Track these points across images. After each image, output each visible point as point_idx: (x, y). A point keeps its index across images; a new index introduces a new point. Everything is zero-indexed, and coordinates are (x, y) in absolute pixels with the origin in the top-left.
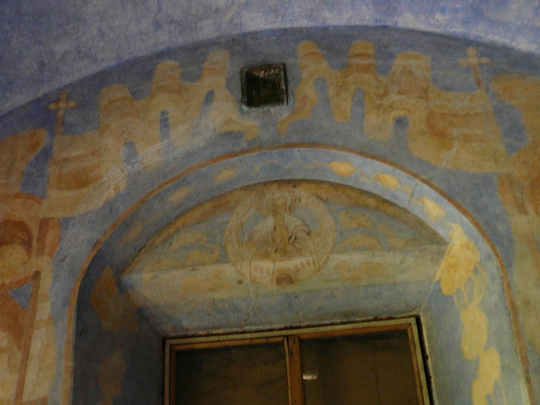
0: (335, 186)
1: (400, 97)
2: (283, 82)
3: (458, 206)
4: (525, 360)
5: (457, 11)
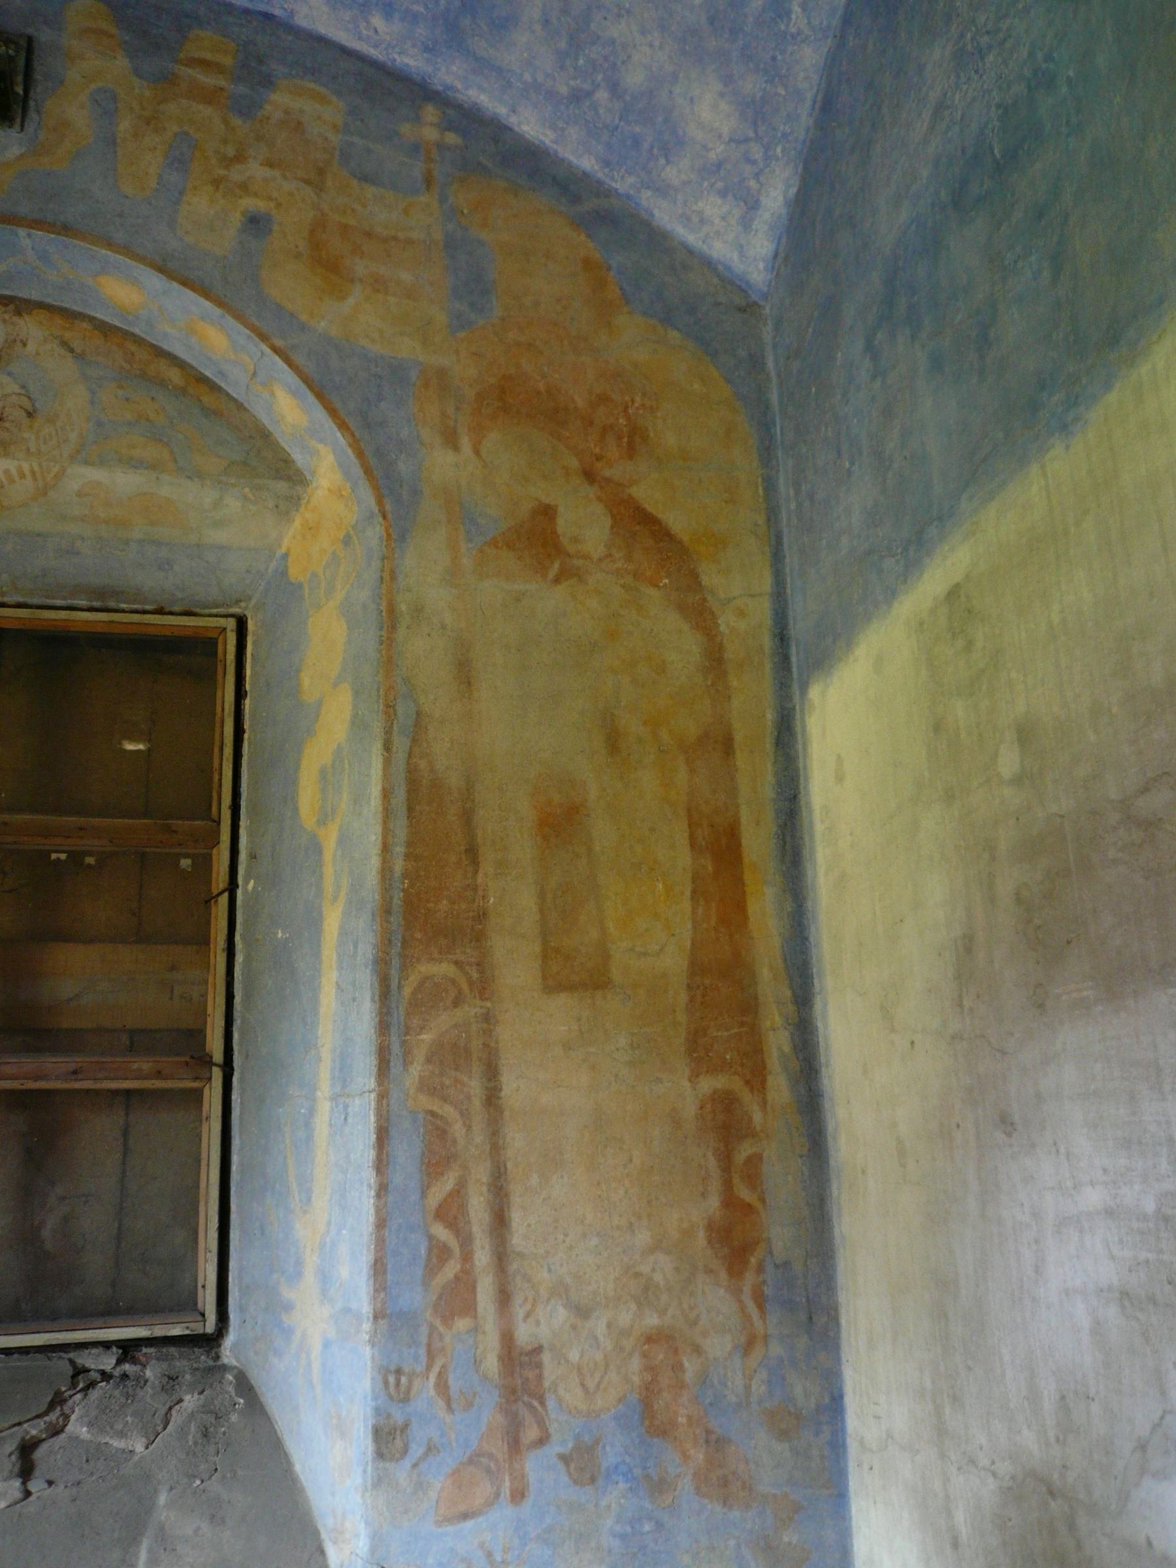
0: (105, 329)
1: (267, 172)
2: (20, 79)
3: (332, 412)
4: (390, 709)
5: (415, 18)
